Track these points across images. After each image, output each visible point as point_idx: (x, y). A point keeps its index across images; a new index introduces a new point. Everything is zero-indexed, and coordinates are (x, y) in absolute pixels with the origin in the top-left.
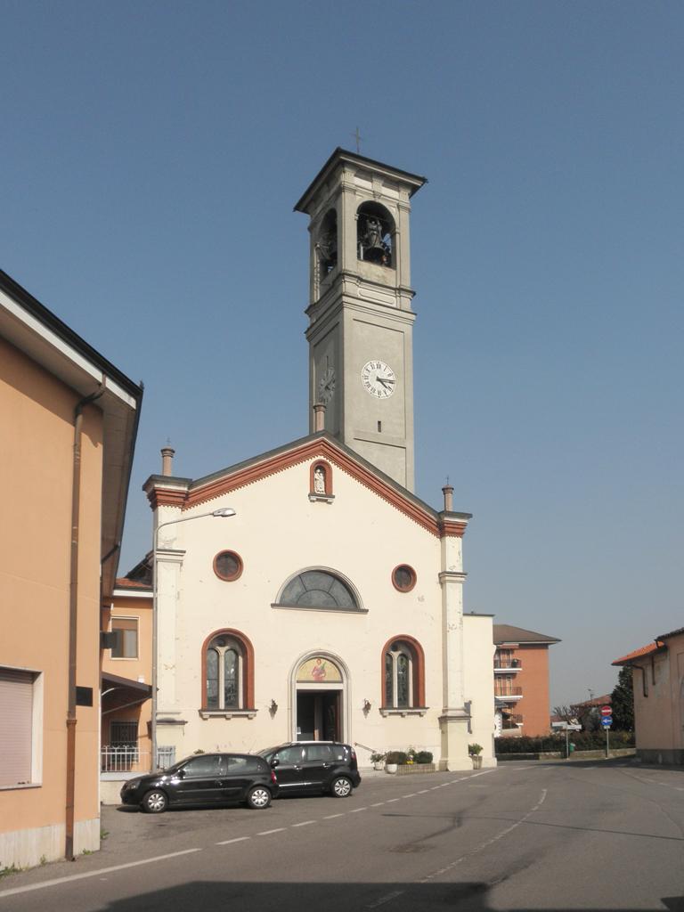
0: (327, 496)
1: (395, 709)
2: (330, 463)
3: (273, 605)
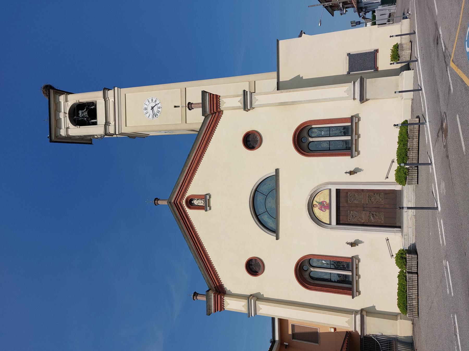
0: (206, 198)
1: (352, 138)
2: (186, 197)
3: (277, 239)
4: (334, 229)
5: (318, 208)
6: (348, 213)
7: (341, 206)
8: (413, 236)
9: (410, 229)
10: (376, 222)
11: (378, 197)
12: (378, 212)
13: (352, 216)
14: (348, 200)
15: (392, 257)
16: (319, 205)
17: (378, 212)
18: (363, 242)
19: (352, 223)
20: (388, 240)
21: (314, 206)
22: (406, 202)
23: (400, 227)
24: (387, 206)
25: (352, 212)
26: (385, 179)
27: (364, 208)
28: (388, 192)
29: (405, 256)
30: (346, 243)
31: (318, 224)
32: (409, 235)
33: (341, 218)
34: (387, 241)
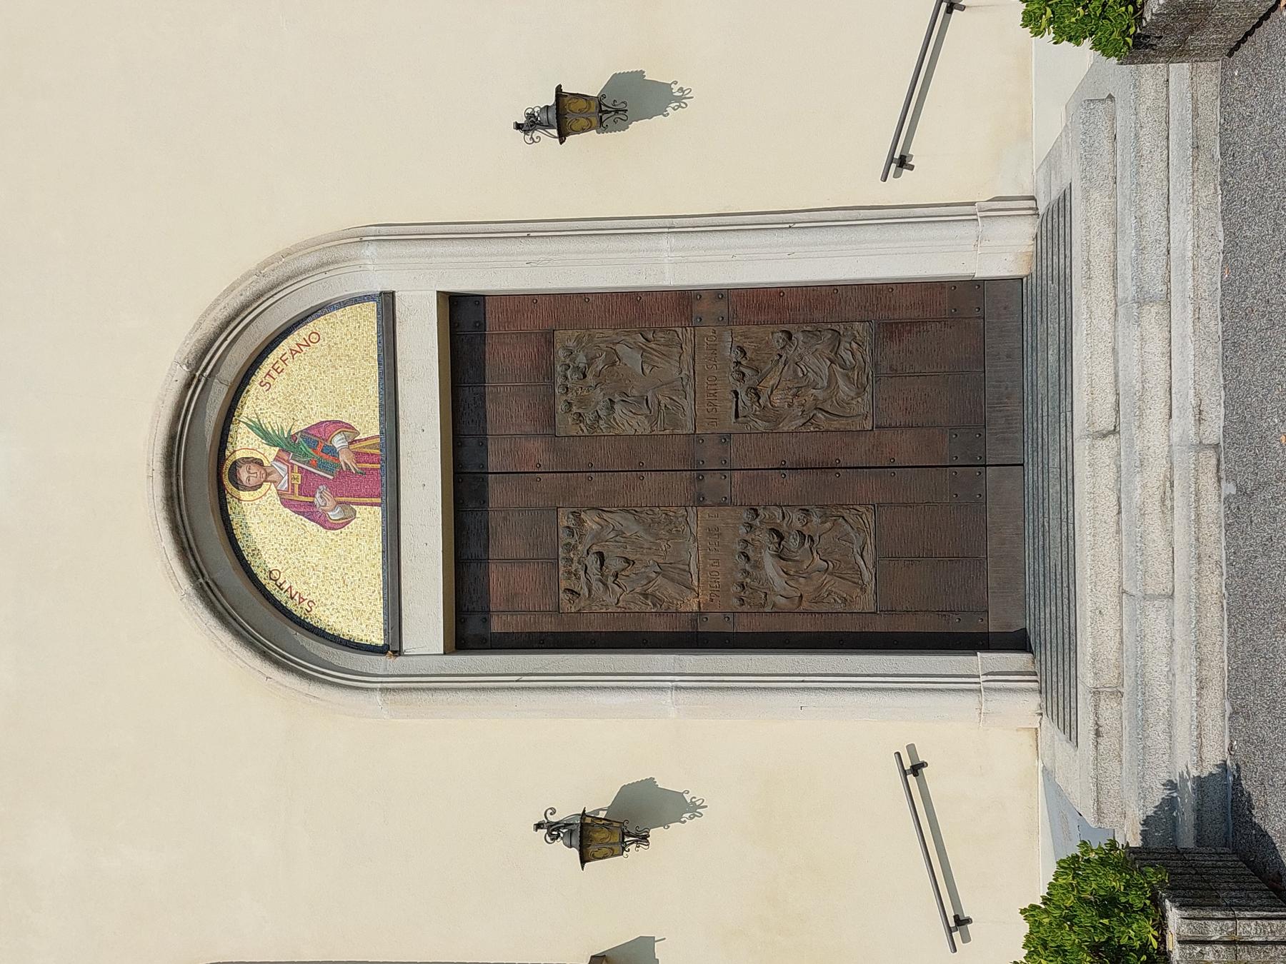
4: (424, 696)
5: (280, 494)
6: (563, 535)
7: (493, 463)
8: (1202, 685)
9: (1156, 620)
10: (805, 605)
11: (816, 364)
12: (822, 507)
13: (592, 562)
14: (560, 407)
15: (956, 935)
16: (281, 469)
17: (822, 507)
18: (694, 809)
19: (596, 626)
20: (917, 769)
21: (243, 475)
22: (1107, 327)
23: (1019, 642)
24: (904, 447)
25: (591, 522)
26: (885, 178)
27: (700, 479)
28: (916, 314)
29: (1151, 935)
30: (539, 826)
31: (265, 655)
32: (1142, 684)
33: (493, 577)
34: (911, 777)
